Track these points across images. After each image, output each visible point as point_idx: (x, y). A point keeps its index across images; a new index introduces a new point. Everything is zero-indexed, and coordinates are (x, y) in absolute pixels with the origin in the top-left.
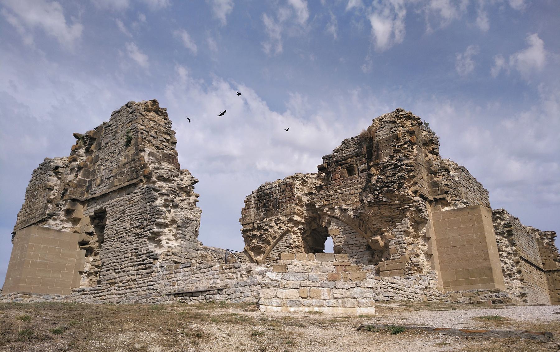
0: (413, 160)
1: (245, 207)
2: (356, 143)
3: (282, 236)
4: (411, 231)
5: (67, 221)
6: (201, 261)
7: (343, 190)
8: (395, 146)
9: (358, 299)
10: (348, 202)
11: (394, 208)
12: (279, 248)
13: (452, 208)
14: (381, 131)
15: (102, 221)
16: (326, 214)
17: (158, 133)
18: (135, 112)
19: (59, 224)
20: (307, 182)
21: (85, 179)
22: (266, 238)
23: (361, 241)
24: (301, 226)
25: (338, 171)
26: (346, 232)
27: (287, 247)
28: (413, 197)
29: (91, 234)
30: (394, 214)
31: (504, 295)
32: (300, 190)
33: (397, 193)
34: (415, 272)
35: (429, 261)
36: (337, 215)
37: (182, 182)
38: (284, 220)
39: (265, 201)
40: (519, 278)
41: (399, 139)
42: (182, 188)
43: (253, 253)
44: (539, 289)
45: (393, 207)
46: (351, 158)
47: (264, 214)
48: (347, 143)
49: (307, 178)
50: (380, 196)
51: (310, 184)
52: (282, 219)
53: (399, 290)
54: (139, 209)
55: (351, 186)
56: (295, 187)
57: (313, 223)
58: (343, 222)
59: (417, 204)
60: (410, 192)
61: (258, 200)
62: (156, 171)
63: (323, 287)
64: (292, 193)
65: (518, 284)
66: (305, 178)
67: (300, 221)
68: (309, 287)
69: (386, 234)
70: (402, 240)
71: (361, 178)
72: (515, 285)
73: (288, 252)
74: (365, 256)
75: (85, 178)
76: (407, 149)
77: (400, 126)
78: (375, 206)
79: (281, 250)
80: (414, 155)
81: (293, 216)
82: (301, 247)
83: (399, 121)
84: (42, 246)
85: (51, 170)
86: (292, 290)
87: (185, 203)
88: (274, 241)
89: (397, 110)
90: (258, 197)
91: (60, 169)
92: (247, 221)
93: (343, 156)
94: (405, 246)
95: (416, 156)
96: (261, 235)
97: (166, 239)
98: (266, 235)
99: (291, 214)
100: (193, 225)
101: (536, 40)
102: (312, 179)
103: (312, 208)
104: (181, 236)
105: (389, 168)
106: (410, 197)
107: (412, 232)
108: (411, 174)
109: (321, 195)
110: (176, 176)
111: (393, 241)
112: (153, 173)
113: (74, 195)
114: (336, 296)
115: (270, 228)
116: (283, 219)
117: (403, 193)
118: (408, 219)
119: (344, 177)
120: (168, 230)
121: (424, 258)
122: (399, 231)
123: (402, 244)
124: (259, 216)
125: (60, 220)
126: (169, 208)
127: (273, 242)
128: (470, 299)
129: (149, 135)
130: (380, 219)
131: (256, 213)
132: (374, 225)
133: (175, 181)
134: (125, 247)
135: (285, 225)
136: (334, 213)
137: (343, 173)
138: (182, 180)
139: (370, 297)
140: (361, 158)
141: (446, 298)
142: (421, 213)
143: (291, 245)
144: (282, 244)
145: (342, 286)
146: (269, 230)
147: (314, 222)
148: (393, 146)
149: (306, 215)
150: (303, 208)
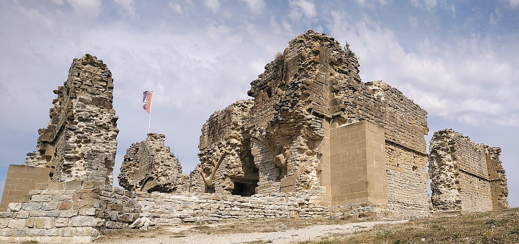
0: (314, 79)
4: (305, 148)
5: (42, 159)
8: (300, 65)
9: (77, 228)
11: (291, 126)
14: (290, 52)
17: (93, 82)
19: (35, 162)
20: (247, 107)
21: (54, 125)
24: (238, 148)
25: (260, 95)
27: (226, 167)
28: (307, 115)
31: (368, 209)
32: (240, 115)
33: (290, 111)
34: (302, 188)
35: (319, 177)
37: (101, 121)
38: (224, 144)
40: (457, 188)
42: (101, 125)
43: (205, 174)
44: (480, 196)
46: (270, 81)
48: (268, 68)
52: (223, 143)
53: (252, 208)
56: (233, 113)
59: (309, 122)
60: (304, 110)
61: (209, 128)
62: (77, 114)
63: (48, 216)
65: (455, 193)
66: (245, 105)
67: (236, 144)
68: (36, 216)
72: (453, 194)
73: (227, 172)
74: (274, 173)
75: (54, 124)
76: (311, 68)
77: (308, 47)
78: (276, 125)
79: (222, 170)
80: (316, 74)
83: (307, 42)
84: (18, 179)
86: (22, 219)
87: (102, 138)
90: (209, 125)
93: (265, 81)
94: (298, 163)
95: (318, 74)
96: (208, 158)
97: (76, 170)
98: (211, 158)
100: (101, 157)
102: (252, 104)
104: (88, 166)
106: (303, 114)
107: (307, 150)
108: (304, 92)
110: (95, 116)
112: (75, 116)
113: (44, 138)
114: (57, 225)
116: (224, 143)
117: (296, 111)
118: (302, 136)
119: (264, 100)
120: (80, 162)
121: (315, 175)
122: (295, 149)
125: (37, 158)
126: (81, 144)
127: (216, 163)
128: (343, 214)
129: (84, 84)
132: (277, 143)
133: (94, 120)
138: (101, 119)
139: (89, 225)
141: (328, 212)
142: (314, 131)
143: (230, 166)
145: (65, 214)
146: (213, 153)
149: (242, 137)
150: (240, 131)
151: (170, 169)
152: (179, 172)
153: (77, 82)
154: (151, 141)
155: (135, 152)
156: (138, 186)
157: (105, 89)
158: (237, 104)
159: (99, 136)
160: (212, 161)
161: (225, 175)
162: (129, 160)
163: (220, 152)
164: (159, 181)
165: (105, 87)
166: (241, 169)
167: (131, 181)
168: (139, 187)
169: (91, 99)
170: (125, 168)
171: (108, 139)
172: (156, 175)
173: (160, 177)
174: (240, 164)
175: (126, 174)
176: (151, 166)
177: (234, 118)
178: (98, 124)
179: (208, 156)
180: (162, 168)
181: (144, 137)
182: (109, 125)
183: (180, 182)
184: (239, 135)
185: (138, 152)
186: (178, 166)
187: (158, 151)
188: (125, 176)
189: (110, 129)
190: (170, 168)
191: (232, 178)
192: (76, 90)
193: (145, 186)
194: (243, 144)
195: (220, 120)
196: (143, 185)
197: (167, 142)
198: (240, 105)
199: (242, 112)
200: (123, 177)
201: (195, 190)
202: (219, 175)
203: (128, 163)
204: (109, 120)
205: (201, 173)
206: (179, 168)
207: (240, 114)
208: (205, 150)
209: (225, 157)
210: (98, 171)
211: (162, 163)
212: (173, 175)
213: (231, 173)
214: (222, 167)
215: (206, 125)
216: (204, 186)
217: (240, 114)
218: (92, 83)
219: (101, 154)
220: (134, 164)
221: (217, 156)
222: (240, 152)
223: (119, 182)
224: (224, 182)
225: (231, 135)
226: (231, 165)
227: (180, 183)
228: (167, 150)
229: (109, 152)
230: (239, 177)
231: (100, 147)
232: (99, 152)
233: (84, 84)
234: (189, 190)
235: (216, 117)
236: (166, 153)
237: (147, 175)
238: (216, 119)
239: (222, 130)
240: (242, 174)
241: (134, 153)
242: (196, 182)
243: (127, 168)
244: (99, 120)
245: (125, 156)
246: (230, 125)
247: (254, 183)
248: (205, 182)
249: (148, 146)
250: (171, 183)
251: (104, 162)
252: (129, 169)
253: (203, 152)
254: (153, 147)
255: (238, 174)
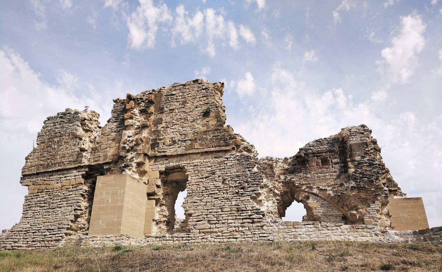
2: (329, 142)
5: (136, 173)
7: (320, 175)
10: (324, 184)
11: (369, 193)
13: (399, 197)
15: (167, 177)
18: (208, 89)
23: (337, 214)
24: (278, 198)
29: (158, 187)
30: (368, 197)
41: (367, 146)
45: (369, 192)
46: (325, 153)
48: (321, 141)
50: (361, 183)
54: (234, 172)
64: (272, 172)
69: (361, 210)
70: (375, 216)
71: (335, 168)
83: (366, 133)
85: (79, 121)
89: (363, 125)
91: (86, 121)
101: (249, 76)
105: (364, 165)
109: (300, 176)
111: (368, 216)
122: (373, 210)
123: (376, 219)
130: (357, 200)
134: (221, 202)
137: (319, 162)
140: (334, 154)
148: (363, 150)
149: (282, 189)
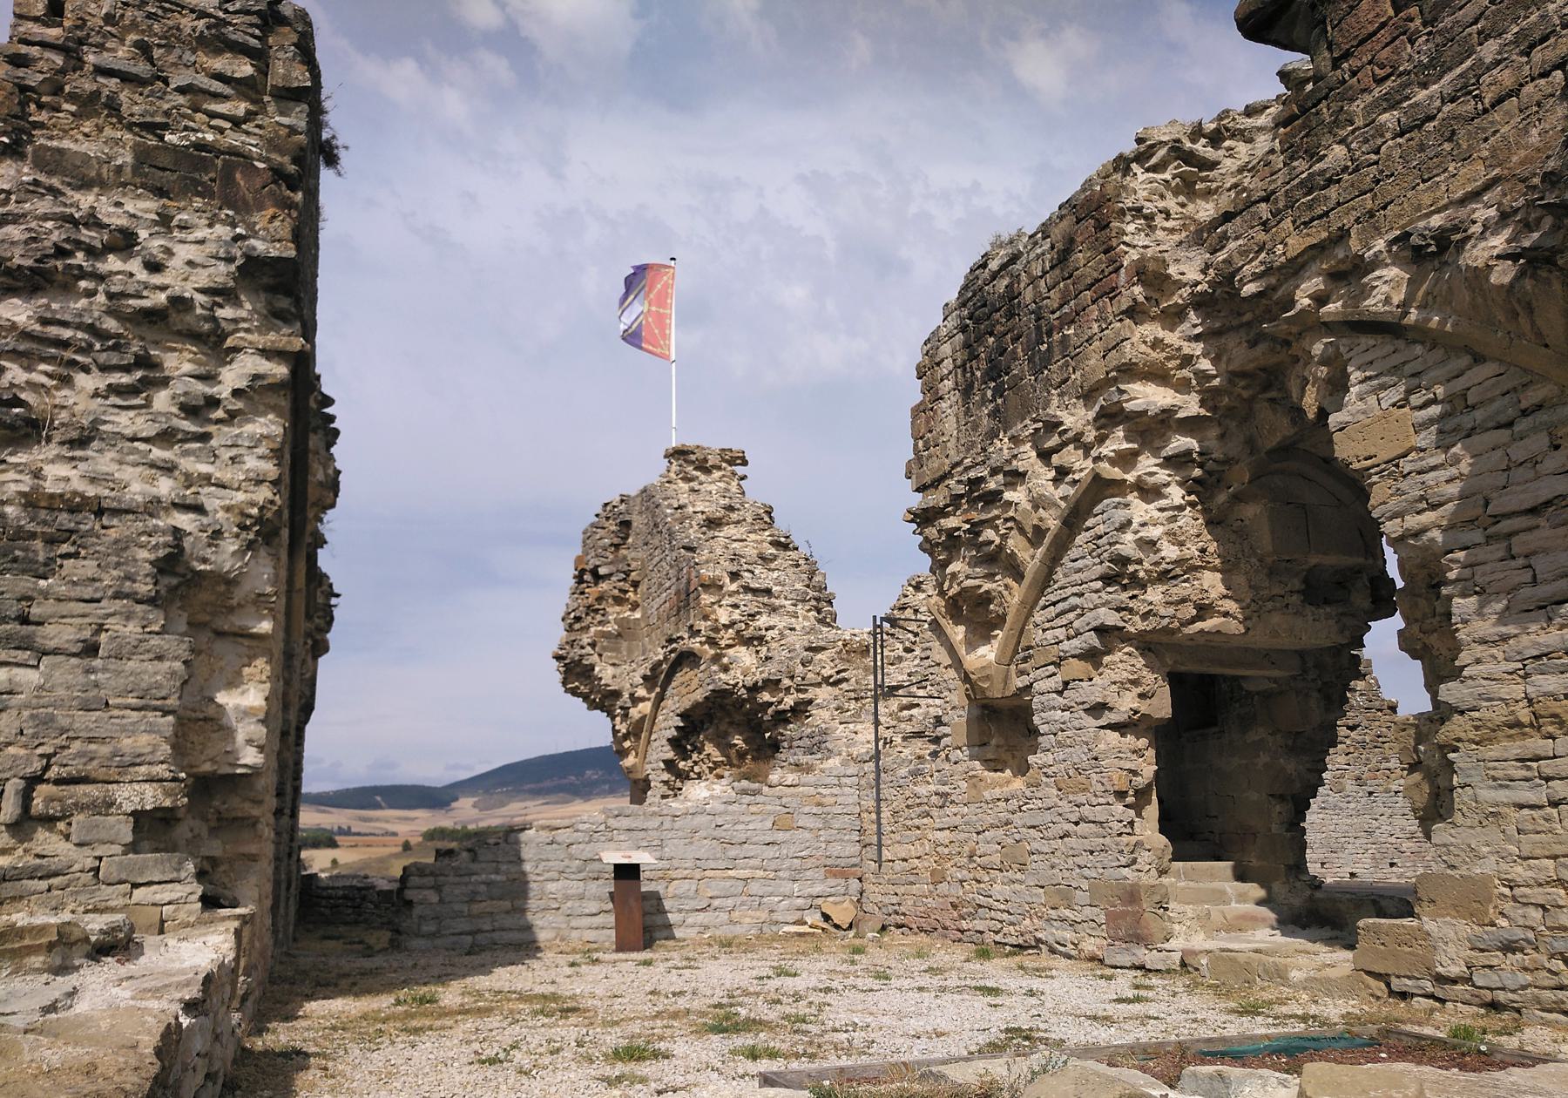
1: (920, 397)
3: (1074, 519)
6: (838, 673)
7: (1422, 95)
12: (1070, 591)
16: (1312, 325)
17: (157, 53)
20: (1214, 165)
22: (998, 541)
24: (1181, 442)
26: (1466, 421)
27: (1108, 580)
32: (1169, 224)
36: (1387, 301)
37: (157, 279)
38: (1079, 427)
39: (991, 340)
43: (961, 629)
47: (994, 414)
49: (1215, 139)
51: (1240, 171)
55: (1484, 36)
56: (1122, 212)
57: (1264, 413)
58: (1433, 347)
66: (1201, 148)
67: (1168, 412)
73: (1119, 610)
79: (1074, 601)
81: (1122, 392)
82: (1196, 568)
88: (1040, 551)
92: (935, 466)
96: (976, 528)
98: (996, 528)
99: (1108, 382)
100: (122, 546)
102: (1250, 141)
103: (1240, 315)
115: (1010, 485)
116: (1076, 418)
124: (975, 427)
127: (1031, 558)
129: (88, 68)
131: (961, 416)
133: (101, 278)
135: (1087, 449)
136: (1366, 291)
143: (1131, 568)
144: (1080, 564)
147: (1272, 400)
149: (1205, 365)
150: (1185, 326)
151: (774, 609)
152: (822, 621)
153: (34, 51)
154: (681, 484)
155: (616, 541)
156: (641, 692)
157: (253, 102)
158: (1142, 147)
159: (132, 390)
160: (1001, 548)
161: (1101, 630)
162: (598, 578)
163: (1056, 481)
164: (726, 669)
165: (245, 87)
166: (1212, 583)
167: (610, 671)
168: (643, 699)
169: (125, 158)
170: (581, 612)
171: (220, 414)
172: (712, 642)
173: (731, 651)
174: (1203, 551)
175: (586, 640)
176: (685, 601)
177: (1135, 243)
178: (131, 302)
179: (976, 516)
180: (736, 606)
181: (648, 470)
182: (226, 313)
183: (826, 672)
184: (1186, 351)
185: (630, 540)
186: (811, 593)
187: (713, 523)
188: (583, 651)
189: (229, 342)
190: (777, 602)
191: (1148, 645)
192: (33, 106)
193: (668, 693)
194: (1214, 409)
195: (1033, 281)
196: (658, 689)
197: (759, 487)
198: (1162, 152)
199: (1182, 199)
200: (575, 653)
201: (906, 713)
202: (1061, 633)
203: (593, 592)
204: (221, 273)
205: (935, 626)
206: (818, 600)
207: (1168, 216)
208: (952, 482)
209: (1089, 513)
210: (97, 663)
211: (732, 581)
212: (791, 638)
213: (1145, 616)
214: (1077, 577)
215: (944, 332)
216: (957, 697)
217: (1168, 216)
218: (150, 60)
219: (118, 529)
220: (616, 592)
221: (1036, 507)
222: (1201, 466)
223: (559, 677)
224: (1097, 680)
225: (1129, 352)
226: (1139, 562)
227: (826, 680)
228: (758, 518)
229: (199, 509)
230: (1202, 641)
231: (127, 473)
232: (100, 512)
233: (88, 68)
234: (872, 718)
235: (1003, 267)
236: (754, 532)
237: (670, 641)
238: (1006, 282)
239: (1056, 337)
240: (1226, 614)
241: (612, 545)
242: (910, 664)
243: (587, 614)
244: (142, 275)
245: (578, 560)
246: (1112, 293)
247: (1305, 671)
248: (966, 678)
249: (670, 506)
250: (780, 680)
251: (144, 588)
252: (599, 617)
253: (937, 498)
254: (690, 509)
255: (1193, 621)
